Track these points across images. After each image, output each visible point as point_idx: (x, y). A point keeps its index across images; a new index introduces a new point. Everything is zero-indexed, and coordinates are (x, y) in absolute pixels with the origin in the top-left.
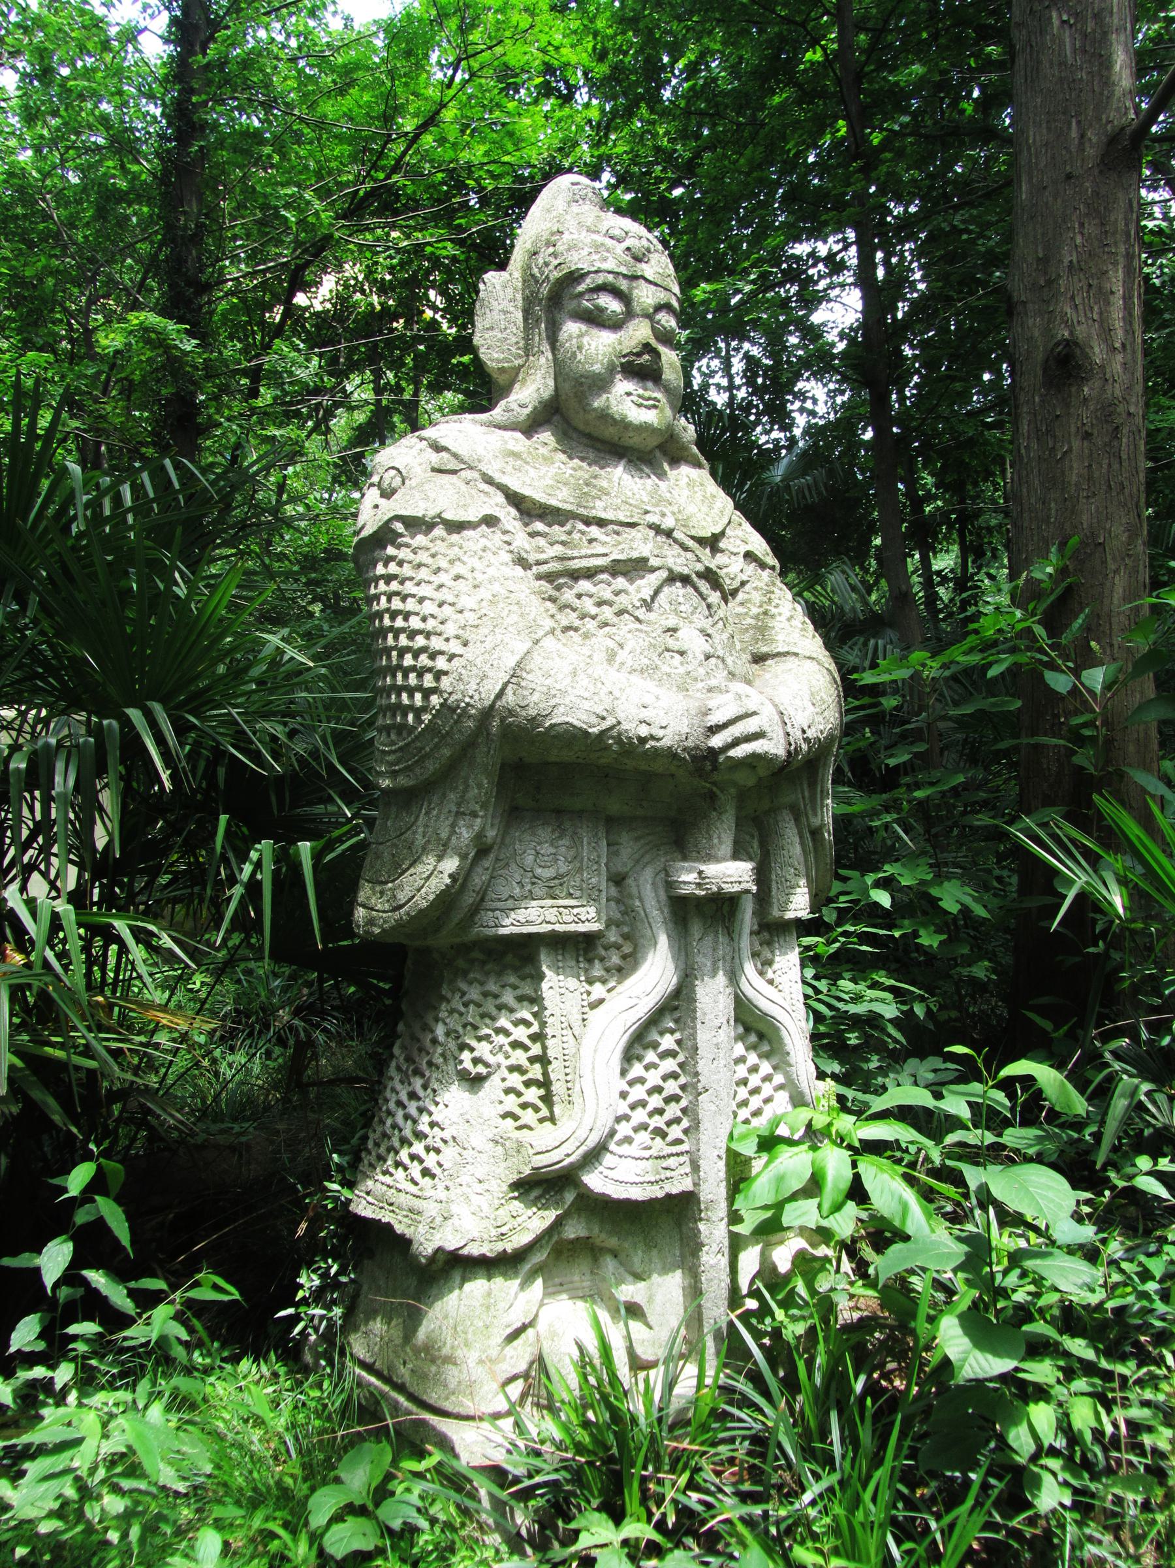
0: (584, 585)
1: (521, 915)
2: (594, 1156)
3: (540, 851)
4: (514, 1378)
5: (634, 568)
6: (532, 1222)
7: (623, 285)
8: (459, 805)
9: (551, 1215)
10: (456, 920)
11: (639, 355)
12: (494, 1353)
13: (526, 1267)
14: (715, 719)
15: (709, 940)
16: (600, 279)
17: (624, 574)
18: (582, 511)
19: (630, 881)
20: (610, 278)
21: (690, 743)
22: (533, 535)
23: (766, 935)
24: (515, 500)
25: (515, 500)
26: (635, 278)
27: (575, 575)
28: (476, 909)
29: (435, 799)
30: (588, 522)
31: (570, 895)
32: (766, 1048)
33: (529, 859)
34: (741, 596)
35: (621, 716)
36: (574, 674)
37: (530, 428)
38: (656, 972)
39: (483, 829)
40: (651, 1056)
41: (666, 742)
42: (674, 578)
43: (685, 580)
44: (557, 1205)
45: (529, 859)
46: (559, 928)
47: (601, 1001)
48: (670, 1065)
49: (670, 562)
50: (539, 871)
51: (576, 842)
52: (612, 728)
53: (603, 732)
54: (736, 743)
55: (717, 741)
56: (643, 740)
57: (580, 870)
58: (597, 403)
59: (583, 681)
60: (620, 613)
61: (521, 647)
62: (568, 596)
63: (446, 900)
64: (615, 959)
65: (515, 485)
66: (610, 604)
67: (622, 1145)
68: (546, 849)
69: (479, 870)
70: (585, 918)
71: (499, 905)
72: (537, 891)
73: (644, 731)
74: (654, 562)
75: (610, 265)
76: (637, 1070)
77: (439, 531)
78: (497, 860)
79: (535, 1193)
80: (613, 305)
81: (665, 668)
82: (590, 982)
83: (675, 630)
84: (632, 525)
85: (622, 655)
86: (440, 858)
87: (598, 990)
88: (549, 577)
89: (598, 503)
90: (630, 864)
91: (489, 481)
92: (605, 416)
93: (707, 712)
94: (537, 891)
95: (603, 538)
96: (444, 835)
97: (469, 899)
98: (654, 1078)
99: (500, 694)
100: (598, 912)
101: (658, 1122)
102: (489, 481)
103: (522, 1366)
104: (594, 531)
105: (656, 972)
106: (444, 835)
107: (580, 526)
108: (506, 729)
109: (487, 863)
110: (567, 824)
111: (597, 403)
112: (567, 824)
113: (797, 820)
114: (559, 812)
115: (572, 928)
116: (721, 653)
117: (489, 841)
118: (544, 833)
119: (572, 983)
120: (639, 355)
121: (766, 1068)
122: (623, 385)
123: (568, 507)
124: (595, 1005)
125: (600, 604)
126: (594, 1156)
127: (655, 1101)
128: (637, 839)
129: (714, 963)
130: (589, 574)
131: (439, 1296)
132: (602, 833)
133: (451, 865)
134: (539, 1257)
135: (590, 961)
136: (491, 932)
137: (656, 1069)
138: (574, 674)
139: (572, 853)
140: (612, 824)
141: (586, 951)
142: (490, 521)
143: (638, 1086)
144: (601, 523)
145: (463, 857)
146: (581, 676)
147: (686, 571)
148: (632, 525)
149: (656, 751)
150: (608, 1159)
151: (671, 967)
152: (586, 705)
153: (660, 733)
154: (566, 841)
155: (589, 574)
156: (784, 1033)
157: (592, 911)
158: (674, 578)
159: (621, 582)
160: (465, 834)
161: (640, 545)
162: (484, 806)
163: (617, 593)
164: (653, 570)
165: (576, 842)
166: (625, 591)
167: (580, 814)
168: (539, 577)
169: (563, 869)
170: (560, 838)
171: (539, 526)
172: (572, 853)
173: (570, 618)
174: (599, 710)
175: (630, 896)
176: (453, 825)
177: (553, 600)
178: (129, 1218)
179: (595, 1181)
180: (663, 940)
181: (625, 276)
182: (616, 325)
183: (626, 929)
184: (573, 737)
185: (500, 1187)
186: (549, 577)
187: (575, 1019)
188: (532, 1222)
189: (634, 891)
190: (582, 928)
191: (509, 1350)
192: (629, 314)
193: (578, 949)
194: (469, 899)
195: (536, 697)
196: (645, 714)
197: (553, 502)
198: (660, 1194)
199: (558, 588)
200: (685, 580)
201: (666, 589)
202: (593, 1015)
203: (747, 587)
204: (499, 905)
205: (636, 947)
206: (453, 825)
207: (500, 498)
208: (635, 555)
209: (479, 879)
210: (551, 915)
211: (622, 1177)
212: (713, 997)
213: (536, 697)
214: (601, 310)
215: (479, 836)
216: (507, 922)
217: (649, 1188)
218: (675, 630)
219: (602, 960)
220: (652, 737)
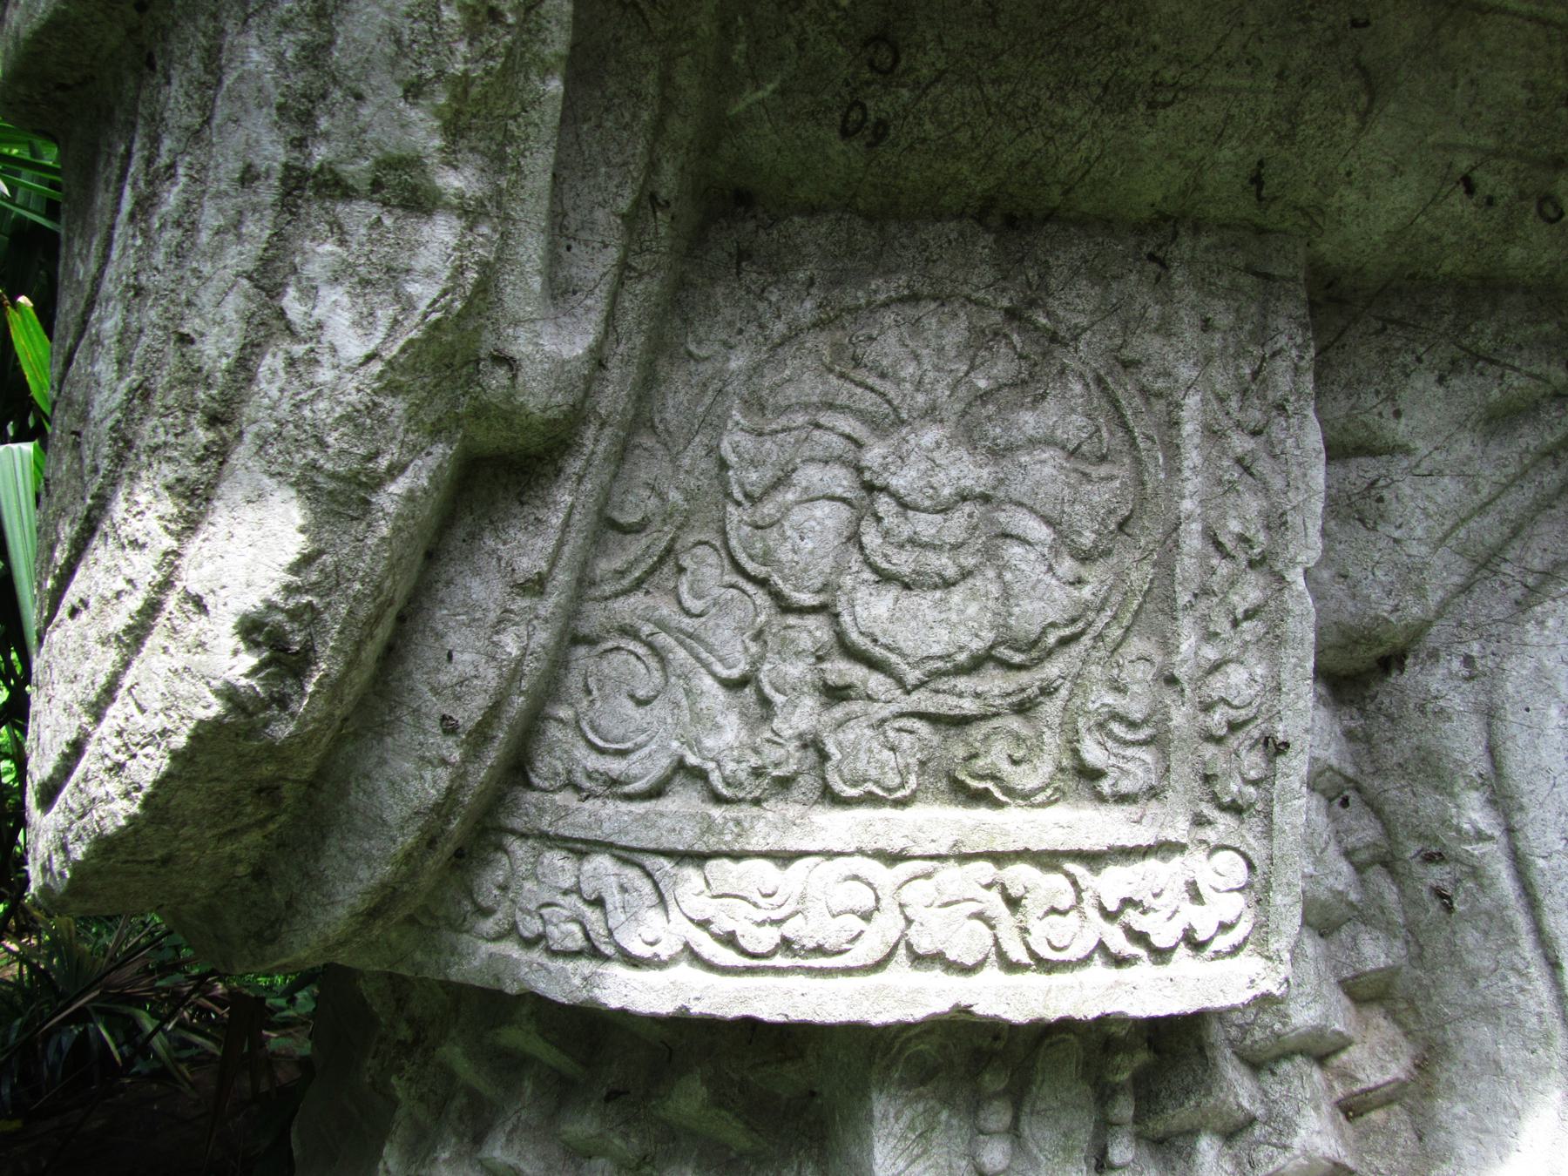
1: (734, 898)
3: (895, 486)
8: (299, 117)
19: (1435, 678)
28: (474, 834)
29: (176, 99)
33: (811, 532)
39: (481, 295)
45: (811, 532)
50: (872, 610)
51: (1130, 422)
57: (1157, 608)
63: (256, 784)
68: (930, 461)
69: (481, 589)
71: (612, 818)
72: (859, 747)
78: (608, 527)
86: (195, 502)
90: (1445, 573)
94: (859, 747)
96: (217, 348)
97: (416, 776)
100: (1258, 889)
106: (217, 348)
109: (531, 544)
110: (1074, 305)
112: (1074, 305)
117: (538, 395)
118: (920, 353)
128: (1499, 421)
131: (986, 1017)
132: (1291, 343)
133: (255, 548)
136: (565, 982)
139: (1106, 491)
141: (1148, 1095)
145: (339, 499)
154: (1063, 414)
160: (348, 334)
162: (474, 120)
165: (1130, 422)
167: (1155, 238)
169: (1043, 593)
170: (1027, 387)
172: (1106, 491)
175: (1432, 769)
176: (268, 278)
183: (1375, 953)
189: (1464, 741)
190: (1148, 994)
194: (416, 776)
204: (612, 818)
205: (1430, 1058)
206: (268, 278)
209: (480, 646)
215: (449, 360)
216: (648, 930)
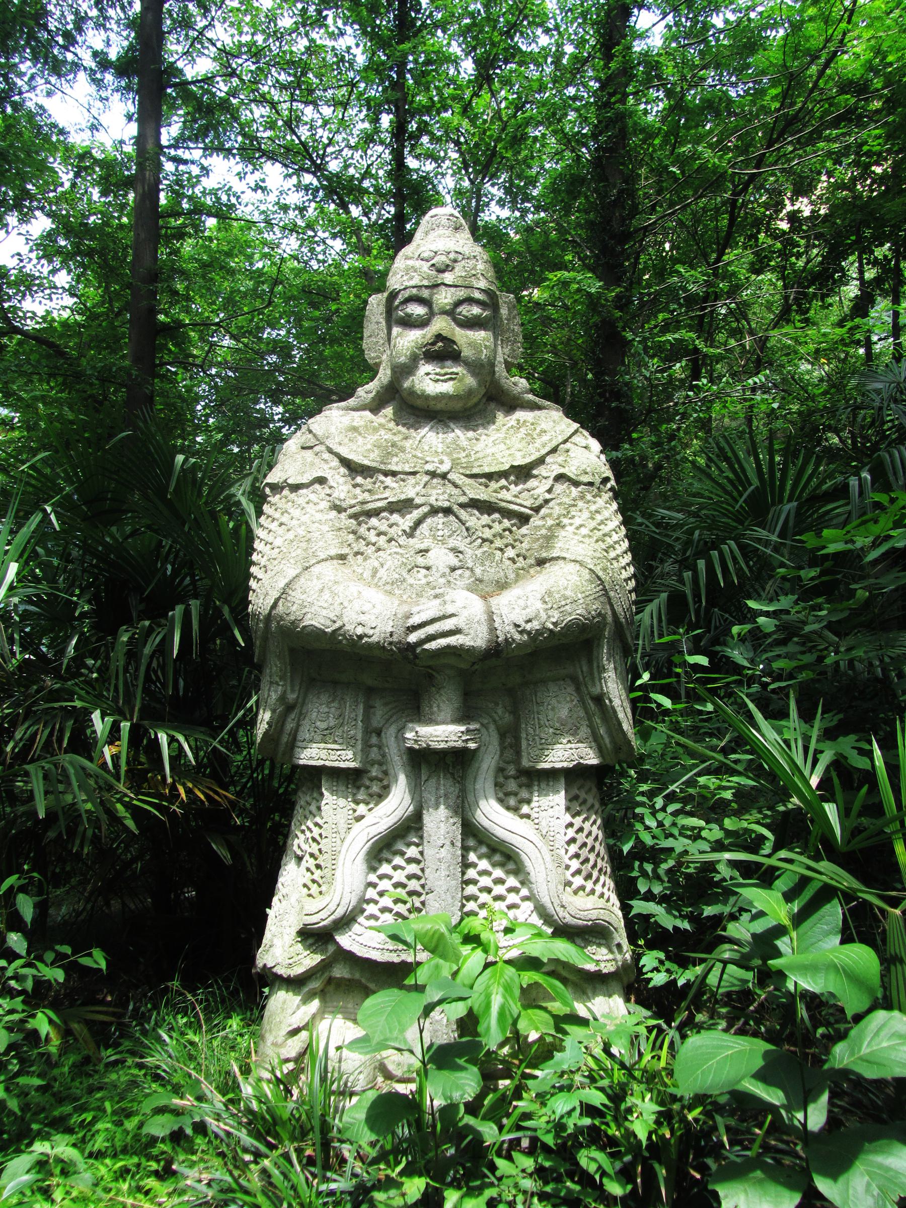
0: (374, 521)
2: (345, 922)
3: (320, 712)
4: (287, 1060)
5: (403, 506)
6: (308, 960)
7: (425, 294)
9: (318, 958)
10: (792, 695)
11: (433, 344)
12: (280, 1040)
13: (306, 989)
14: (415, 620)
15: (433, 782)
16: (407, 294)
17: (399, 511)
18: (383, 467)
20: (414, 291)
21: (395, 639)
22: (355, 486)
23: (524, 780)
24: (346, 463)
25: (346, 463)
26: (436, 286)
27: (370, 514)
30: (386, 474)
31: (335, 742)
32: (511, 866)
34: (543, 511)
35: (346, 620)
36: (322, 591)
37: (375, 407)
38: (397, 803)
40: (398, 861)
41: (375, 639)
42: (435, 511)
43: (447, 511)
44: (322, 952)
46: (328, 763)
47: (363, 817)
48: (413, 868)
49: (432, 500)
52: (340, 628)
53: (334, 631)
54: (431, 638)
55: (413, 638)
56: (361, 637)
57: (342, 725)
58: (406, 384)
59: (326, 595)
60: (390, 541)
61: (292, 573)
62: (362, 530)
64: (375, 789)
65: (345, 452)
66: (385, 534)
67: (429, 917)
68: (324, 709)
70: (346, 758)
73: (360, 631)
74: (418, 501)
75: (416, 281)
76: (385, 868)
77: (286, 492)
79: (310, 941)
80: (418, 310)
81: (411, 581)
82: (357, 803)
83: (427, 551)
84: (414, 473)
85: (382, 573)
87: (362, 809)
88: (354, 516)
89: (395, 459)
91: (330, 451)
92: (412, 392)
93: (408, 616)
95: (394, 485)
97: (285, 739)
98: (399, 876)
99: (274, 606)
101: (401, 908)
102: (330, 451)
103: (293, 1054)
104: (389, 481)
105: (397, 803)
107: (381, 477)
108: (280, 627)
111: (406, 384)
113: (578, 689)
114: (335, 683)
115: (336, 764)
116: (470, 565)
118: (324, 698)
119: (342, 802)
120: (433, 344)
121: (512, 881)
122: (425, 368)
123: (374, 464)
124: (359, 818)
125: (379, 535)
126: (345, 922)
127: (401, 893)
128: (386, 704)
129: (437, 799)
130: (376, 513)
132: (361, 699)
134: (315, 984)
135: (358, 788)
137: (397, 870)
138: (322, 591)
140: (370, 692)
141: (355, 781)
142: (321, 481)
143: (385, 881)
144: (394, 474)
146: (326, 591)
147: (446, 504)
148: (414, 473)
149: (370, 646)
150: (356, 928)
151: (408, 799)
152: (324, 613)
153: (371, 632)
154: (335, 704)
155: (376, 513)
156: (524, 857)
157: (350, 754)
158: (435, 511)
159: (396, 517)
161: (410, 490)
163: (391, 526)
164: (418, 506)
166: (396, 524)
168: (350, 517)
171: (359, 480)
173: (361, 546)
174: (332, 616)
177: (354, 532)
178: (893, 852)
179: (345, 940)
180: (402, 779)
181: (427, 287)
182: (422, 323)
184: (317, 634)
185: (293, 931)
186: (354, 516)
187: (343, 826)
188: (308, 960)
190: (343, 765)
191: (290, 1041)
192: (431, 314)
193: (350, 780)
195: (294, 608)
196: (362, 618)
197: (366, 462)
198: (396, 960)
199: (359, 524)
200: (447, 511)
201: (429, 520)
202: (357, 826)
203: (551, 504)
207: (335, 462)
208: (403, 497)
209: (290, 725)
210: (323, 754)
211: (365, 941)
212: (440, 823)
213: (294, 608)
214: (409, 316)
217: (387, 954)
218: (427, 551)
219: (368, 788)
220: (366, 635)
